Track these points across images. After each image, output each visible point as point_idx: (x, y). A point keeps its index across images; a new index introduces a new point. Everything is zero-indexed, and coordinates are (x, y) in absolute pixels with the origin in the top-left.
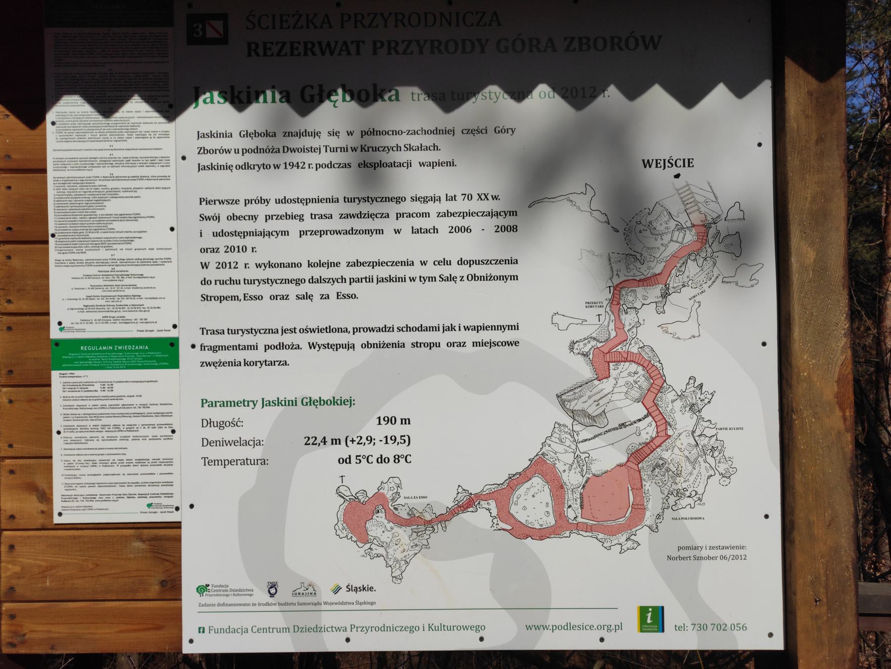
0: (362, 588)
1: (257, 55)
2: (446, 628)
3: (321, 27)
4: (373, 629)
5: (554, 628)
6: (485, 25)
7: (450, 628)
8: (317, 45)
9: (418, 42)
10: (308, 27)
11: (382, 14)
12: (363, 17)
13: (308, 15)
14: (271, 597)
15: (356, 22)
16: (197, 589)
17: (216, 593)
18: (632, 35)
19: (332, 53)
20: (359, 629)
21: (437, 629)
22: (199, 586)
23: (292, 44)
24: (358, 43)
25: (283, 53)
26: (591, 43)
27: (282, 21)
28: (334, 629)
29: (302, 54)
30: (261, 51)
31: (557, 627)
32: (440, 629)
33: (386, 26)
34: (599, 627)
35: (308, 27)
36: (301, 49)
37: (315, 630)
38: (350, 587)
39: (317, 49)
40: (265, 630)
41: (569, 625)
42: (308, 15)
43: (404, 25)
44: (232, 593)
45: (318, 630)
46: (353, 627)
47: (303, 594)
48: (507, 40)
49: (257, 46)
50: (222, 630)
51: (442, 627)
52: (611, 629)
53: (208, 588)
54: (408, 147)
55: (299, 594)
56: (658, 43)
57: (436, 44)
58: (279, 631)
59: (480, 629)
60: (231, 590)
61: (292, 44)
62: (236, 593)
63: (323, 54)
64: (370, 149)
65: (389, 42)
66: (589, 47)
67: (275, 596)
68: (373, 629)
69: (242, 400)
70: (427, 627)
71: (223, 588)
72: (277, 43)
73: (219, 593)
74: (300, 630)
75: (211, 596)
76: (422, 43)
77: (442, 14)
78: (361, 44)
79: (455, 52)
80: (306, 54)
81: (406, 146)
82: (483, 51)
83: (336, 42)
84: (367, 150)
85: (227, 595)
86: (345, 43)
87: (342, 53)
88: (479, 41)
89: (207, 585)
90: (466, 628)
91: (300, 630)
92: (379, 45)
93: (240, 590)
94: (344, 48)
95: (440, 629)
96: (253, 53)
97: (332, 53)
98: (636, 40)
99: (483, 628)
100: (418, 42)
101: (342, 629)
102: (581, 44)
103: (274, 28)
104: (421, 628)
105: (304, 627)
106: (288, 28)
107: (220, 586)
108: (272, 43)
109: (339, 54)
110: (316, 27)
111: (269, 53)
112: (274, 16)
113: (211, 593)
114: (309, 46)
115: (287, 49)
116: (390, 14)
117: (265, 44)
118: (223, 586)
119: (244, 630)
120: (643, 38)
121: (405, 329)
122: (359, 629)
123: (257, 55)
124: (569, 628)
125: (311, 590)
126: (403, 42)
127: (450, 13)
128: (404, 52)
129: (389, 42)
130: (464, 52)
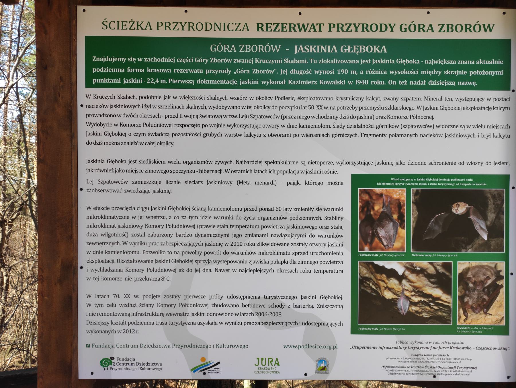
2: (226, 346)
3: (146, 29)
4: (185, 346)
5: (300, 347)
6: (240, 30)
8: (297, 26)
9: (355, 25)
10: (138, 29)
11: (181, 23)
13: (138, 22)
15: (166, 26)
16: (101, 362)
17: (121, 367)
19: (305, 30)
21: (221, 347)
22: (103, 359)
23: (282, 24)
24: (320, 25)
25: (277, 30)
26: (454, 28)
29: (288, 30)
30: (264, 28)
32: (223, 347)
34: (325, 347)
35: (138, 29)
36: (288, 27)
39: (297, 28)
40: (124, 346)
42: (138, 22)
43: (194, 30)
44: (139, 367)
46: (174, 345)
48: (406, 25)
49: (263, 25)
50: (100, 346)
52: (331, 348)
53: (113, 361)
54: (120, 96)
58: (132, 347)
59: (245, 347)
61: (282, 24)
62: (143, 367)
63: (300, 30)
64: (98, 97)
65: (338, 25)
66: (453, 30)
68: (185, 346)
69: (275, 225)
70: (215, 346)
72: (274, 24)
73: (125, 367)
75: (116, 369)
76: (357, 25)
77: (215, 23)
78: (322, 25)
79: (457, 25)
81: (119, 96)
82: (392, 31)
83: (308, 24)
84: (97, 98)
85: (134, 369)
86: (313, 25)
87: (311, 30)
88: (390, 25)
89: (112, 358)
90: (237, 346)
92: (332, 26)
93: (147, 364)
94: (312, 28)
95: (223, 347)
96: (260, 29)
97: (305, 30)
99: (247, 346)
100: (355, 25)
102: (448, 28)
103: (118, 29)
104: (212, 346)
106: (127, 29)
107: (126, 359)
108: (271, 24)
109: (310, 31)
110: (142, 29)
111: (269, 29)
112: (118, 22)
113: (116, 367)
114: (292, 26)
115: (280, 27)
116: (186, 23)
117: (267, 24)
118: (129, 360)
120: (484, 25)
123: (263, 30)
126: (346, 24)
127: (220, 23)
128: (347, 31)
129: (338, 25)
130: (381, 31)
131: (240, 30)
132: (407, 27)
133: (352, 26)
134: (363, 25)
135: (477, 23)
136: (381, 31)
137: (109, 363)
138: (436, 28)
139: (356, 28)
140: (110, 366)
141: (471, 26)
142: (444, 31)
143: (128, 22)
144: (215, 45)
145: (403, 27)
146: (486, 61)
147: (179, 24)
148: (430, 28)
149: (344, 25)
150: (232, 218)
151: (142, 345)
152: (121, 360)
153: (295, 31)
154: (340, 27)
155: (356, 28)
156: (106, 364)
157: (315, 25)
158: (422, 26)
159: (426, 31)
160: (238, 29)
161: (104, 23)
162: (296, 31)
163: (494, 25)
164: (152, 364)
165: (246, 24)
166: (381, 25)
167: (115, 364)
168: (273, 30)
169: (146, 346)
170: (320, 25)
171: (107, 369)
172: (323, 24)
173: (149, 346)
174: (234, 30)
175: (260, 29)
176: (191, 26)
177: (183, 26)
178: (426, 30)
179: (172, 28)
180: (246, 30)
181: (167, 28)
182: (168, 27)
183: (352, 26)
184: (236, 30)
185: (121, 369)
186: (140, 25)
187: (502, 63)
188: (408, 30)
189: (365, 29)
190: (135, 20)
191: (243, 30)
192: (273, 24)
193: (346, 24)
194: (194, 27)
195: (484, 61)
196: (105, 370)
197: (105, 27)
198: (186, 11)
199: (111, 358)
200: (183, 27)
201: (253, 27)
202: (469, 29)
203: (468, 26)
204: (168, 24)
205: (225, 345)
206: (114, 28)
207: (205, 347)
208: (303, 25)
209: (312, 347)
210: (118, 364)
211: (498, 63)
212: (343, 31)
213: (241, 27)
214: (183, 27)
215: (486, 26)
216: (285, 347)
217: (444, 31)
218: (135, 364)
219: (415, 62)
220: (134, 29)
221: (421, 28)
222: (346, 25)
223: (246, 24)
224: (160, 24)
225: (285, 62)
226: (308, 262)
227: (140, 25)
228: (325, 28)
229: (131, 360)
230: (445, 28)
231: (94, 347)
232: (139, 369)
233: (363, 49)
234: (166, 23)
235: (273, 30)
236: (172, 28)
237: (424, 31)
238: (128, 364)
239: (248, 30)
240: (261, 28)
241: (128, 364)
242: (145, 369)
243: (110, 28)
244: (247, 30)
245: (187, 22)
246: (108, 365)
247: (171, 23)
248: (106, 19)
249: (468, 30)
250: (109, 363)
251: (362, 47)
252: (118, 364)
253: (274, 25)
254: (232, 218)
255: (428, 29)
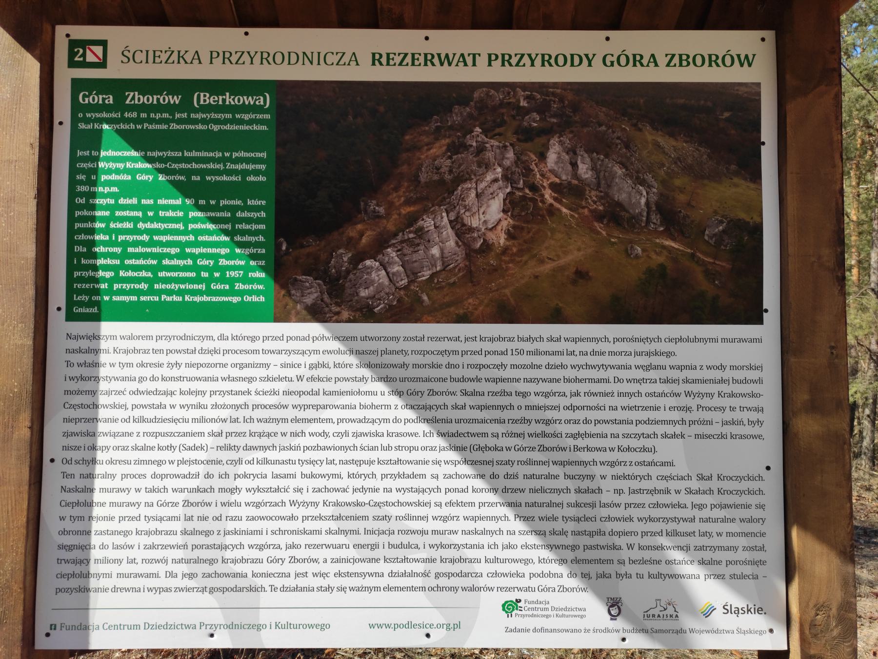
0: (745, 609)
2: (292, 626)
3: (191, 63)
4: (222, 626)
5: (396, 626)
6: (345, 64)
7: (297, 627)
8: (436, 57)
9: (529, 55)
10: (179, 62)
11: (248, 53)
12: (231, 54)
13: (179, 52)
14: (611, 619)
15: (224, 58)
16: (503, 605)
17: (530, 613)
18: (729, 53)
19: (450, 64)
21: (283, 627)
22: (506, 602)
23: (413, 55)
26: (690, 60)
27: (154, 57)
28: (183, 626)
29: (423, 64)
30: (384, 60)
32: (286, 627)
34: (439, 626)
35: (179, 62)
36: (422, 60)
37: (165, 627)
39: (436, 60)
41: (410, 623)
42: (179, 52)
43: (269, 63)
44: (555, 612)
45: (168, 627)
47: (659, 616)
48: (612, 55)
49: (381, 56)
50: (74, 627)
51: (289, 626)
52: (450, 627)
53: (519, 604)
55: (654, 616)
56: (752, 61)
58: (129, 628)
59: (325, 627)
60: (554, 609)
62: (560, 613)
63: (442, 64)
65: (503, 55)
66: (688, 64)
70: (273, 626)
72: (399, 54)
73: (535, 613)
74: (150, 627)
77: (304, 53)
78: (477, 56)
82: (590, 65)
83: (454, 54)
85: (547, 616)
86: (462, 55)
88: (587, 56)
90: (311, 626)
91: (150, 627)
93: (566, 609)
94: (461, 60)
95: (286, 627)
96: (377, 62)
97: (450, 64)
98: (732, 58)
99: (328, 626)
100: (529, 55)
101: (192, 626)
102: (413, 59)
103: (147, 62)
104: (268, 627)
105: (173, 624)
108: (395, 54)
109: (457, 65)
110: (186, 63)
111: (391, 62)
112: (147, 51)
113: (523, 612)
114: (429, 57)
115: (409, 59)
116: (256, 52)
117: (388, 55)
118: (541, 603)
119: (95, 627)
120: (739, 56)
123: (381, 64)
124: (410, 627)
125: (670, 610)
126: (516, 55)
127: (312, 53)
128: (517, 65)
129: (503, 55)
131: (345, 64)
132: (615, 59)
133: (526, 57)
134: (543, 55)
135: (728, 53)
136: (572, 65)
137: (513, 607)
138: (662, 60)
139: (533, 61)
140: (515, 611)
141: (550, 57)
143: (164, 52)
144: (87, 93)
145: (609, 59)
148: (652, 60)
149: (513, 56)
150: (277, 394)
151: (147, 625)
152: (530, 603)
153: (433, 64)
154: (506, 60)
155: (533, 61)
156: (509, 609)
158: (638, 58)
159: (645, 65)
160: (342, 62)
162: (435, 65)
163: (754, 55)
166: (572, 56)
167: (523, 609)
168: (397, 64)
169: (154, 626)
170: (474, 55)
171: (511, 616)
172: (479, 55)
173: (159, 627)
174: (335, 63)
175: (377, 62)
176: (266, 58)
178: (645, 64)
179: (514, 63)
180: (353, 63)
181: (227, 61)
182: (228, 58)
185: (531, 616)
186: (182, 57)
188: (615, 63)
189: (637, 63)
190: (175, 48)
191: (349, 64)
192: (164, 52)
193: (516, 55)
194: (270, 59)
196: (508, 617)
197: (126, 60)
198: (246, 34)
199: (516, 600)
200: (252, 59)
202: (548, 61)
203: (714, 58)
205: (290, 624)
206: (331, 63)
207: (256, 627)
208: (447, 56)
209: (418, 626)
210: (526, 609)
212: (510, 65)
213: (346, 59)
214: (252, 59)
215: (742, 58)
216: (372, 626)
217: (675, 64)
218: (550, 609)
220: (173, 62)
221: (637, 60)
222: (516, 56)
226: (541, 463)
227: (182, 57)
228: (482, 61)
229: (544, 603)
230: (676, 60)
231: (64, 629)
232: (555, 616)
233: (206, 98)
234: (224, 52)
236: (514, 63)
237: (642, 65)
238: (539, 609)
239: (357, 64)
240: (715, 61)
241: (539, 609)
242: (563, 616)
244: (355, 63)
245: (259, 50)
246: (513, 610)
248: (127, 47)
251: (205, 96)
252: (526, 609)
253: (399, 55)
254: (277, 394)
255: (649, 62)
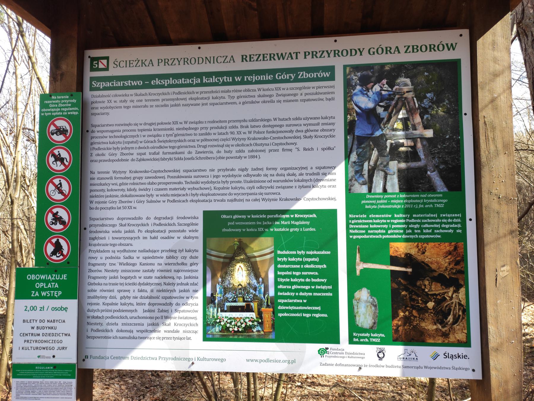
0: (457, 356)
1: (246, 61)
3: (148, 66)
7: (208, 360)
8: (276, 55)
9: (327, 51)
10: (142, 66)
11: (177, 59)
13: (142, 60)
14: (379, 360)
15: (165, 62)
16: (319, 351)
17: (334, 355)
19: (283, 59)
20: (163, 359)
22: (320, 349)
23: (264, 55)
24: (297, 53)
25: (259, 60)
26: (419, 48)
27: (130, 64)
30: (248, 59)
31: (262, 361)
33: (179, 64)
35: (142, 66)
38: (447, 355)
39: (276, 57)
42: (142, 60)
43: (188, 64)
44: (347, 355)
47: (406, 358)
49: (246, 56)
53: (327, 350)
57: (337, 52)
60: (346, 353)
61: (264, 55)
62: (350, 356)
63: (279, 59)
65: (313, 52)
66: (418, 51)
67: (383, 359)
71: (340, 352)
73: (336, 355)
75: (330, 357)
76: (329, 52)
77: (206, 58)
78: (298, 53)
80: (270, 60)
82: (361, 55)
83: (286, 53)
85: (343, 357)
86: (290, 53)
87: (289, 58)
88: (359, 49)
90: (216, 360)
92: (307, 54)
93: (354, 353)
94: (290, 56)
96: (244, 60)
97: (283, 59)
100: (327, 51)
103: (126, 67)
108: (254, 55)
109: (287, 59)
110: (146, 66)
112: (126, 61)
113: (330, 355)
114: (272, 56)
117: (250, 56)
118: (340, 350)
120: (447, 44)
121: (318, 199)
122: (163, 359)
123: (246, 61)
125: (413, 356)
126: (320, 52)
128: (320, 57)
129: (313, 52)
132: (375, 50)
133: (325, 52)
134: (335, 51)
136: (351, 55)
137: (324, 352)
140: (325, 354)
141: (434, 46)
142: (261, 60)
146: (228, 78)
147: (176, 60)
148: (396, 50)
152: (333, 350)
157: (292, 54)
158: (388, 49)
159: (393, 53)
160: (226, 61)
161: (115, 63)
163: (456, 44)
164: (357, 354)
165: (232, 56)
166: (351, 50)
172: (299, 53)
174: (222, 62)
175: (244, 60)
177: (361, 51)
180: (232, 61)
181: (166, 64)
183: (325, 52)
184: (224, 62)
187: (271, 78)
188: (376, 53)
190: (140, 59)
191: (230, 62)
194: (189, 62)
195: (225, 77)
197: (115, 66)
199: (326, 348)
200: (179, 62)
201: (238, 59)
202: (338, 54)
203: (432, 46)
204: (167, 61)
210: (331, 353)
211: (266, 78)
213: (228, 59)
214: (179, 62)
219: (206, 80)
223: (151, 60)
224: (160, 61)
225: (94, 85)
230: (411, 49)
234: (165, 59)
235: (255, 60)
237: (391, 53)
240: (245, 59)
242: (352, 357)
243: (217, 62)
244: (233, 61)
245: (183, 57)
246: (324, 353)
247: (170, 60)
249: (432, 50)
250: (324, 352)
252: (331, 353)
255: (395, 51)
